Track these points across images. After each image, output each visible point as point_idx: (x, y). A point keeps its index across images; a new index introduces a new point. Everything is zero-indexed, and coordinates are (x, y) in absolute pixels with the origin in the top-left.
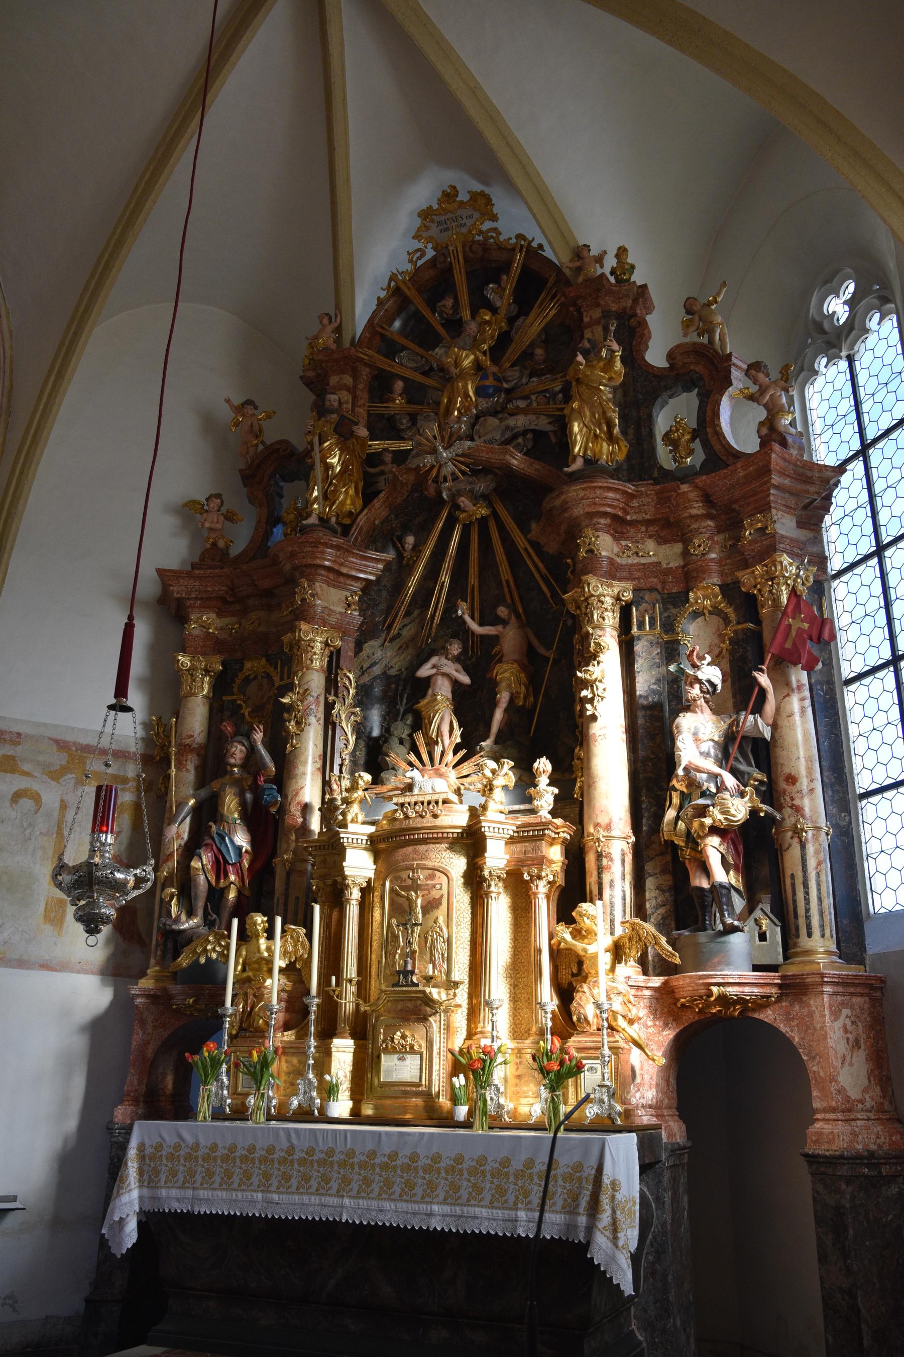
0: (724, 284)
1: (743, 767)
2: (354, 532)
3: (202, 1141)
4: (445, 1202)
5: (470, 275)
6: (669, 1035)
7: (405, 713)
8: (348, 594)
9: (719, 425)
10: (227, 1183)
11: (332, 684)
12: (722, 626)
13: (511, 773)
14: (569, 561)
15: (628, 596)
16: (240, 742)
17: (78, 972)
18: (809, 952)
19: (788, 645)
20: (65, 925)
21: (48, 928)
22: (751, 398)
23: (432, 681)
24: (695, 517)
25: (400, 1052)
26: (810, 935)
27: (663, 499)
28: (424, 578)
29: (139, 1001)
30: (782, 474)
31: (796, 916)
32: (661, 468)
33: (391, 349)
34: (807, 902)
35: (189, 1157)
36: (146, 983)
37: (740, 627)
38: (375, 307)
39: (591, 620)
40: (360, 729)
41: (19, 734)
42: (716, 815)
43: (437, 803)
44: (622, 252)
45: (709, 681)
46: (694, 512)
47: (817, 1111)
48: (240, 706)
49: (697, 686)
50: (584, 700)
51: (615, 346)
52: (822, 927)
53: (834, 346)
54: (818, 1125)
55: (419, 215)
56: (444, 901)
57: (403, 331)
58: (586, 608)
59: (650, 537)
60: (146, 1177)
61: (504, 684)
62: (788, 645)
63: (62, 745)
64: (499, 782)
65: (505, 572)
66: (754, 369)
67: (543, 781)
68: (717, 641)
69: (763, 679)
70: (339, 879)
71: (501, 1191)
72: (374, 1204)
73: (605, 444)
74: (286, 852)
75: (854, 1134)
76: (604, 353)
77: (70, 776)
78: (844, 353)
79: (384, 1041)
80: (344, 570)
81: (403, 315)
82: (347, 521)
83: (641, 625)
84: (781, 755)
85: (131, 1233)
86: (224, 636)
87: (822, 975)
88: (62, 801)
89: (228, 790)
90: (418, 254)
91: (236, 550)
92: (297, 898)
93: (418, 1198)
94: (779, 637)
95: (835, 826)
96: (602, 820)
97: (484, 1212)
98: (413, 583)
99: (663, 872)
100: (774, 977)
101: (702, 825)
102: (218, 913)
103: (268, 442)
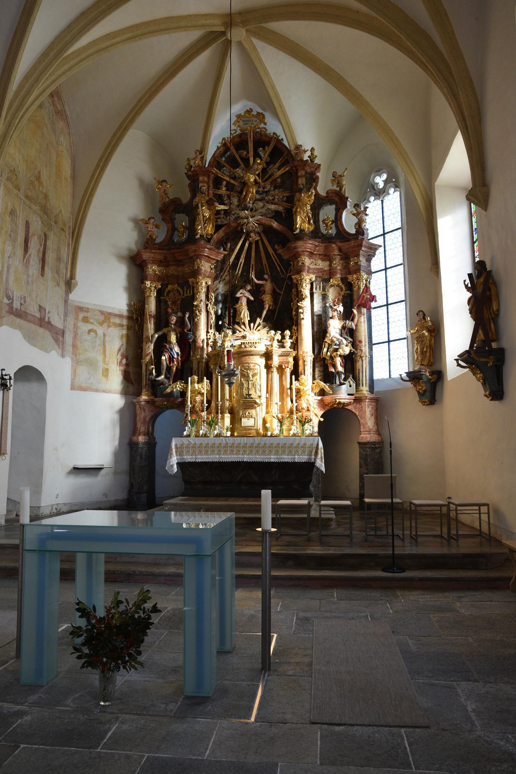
0: (346, 169)
1: (346, 337)
2: (212, 241)
3: (197, 442)
4: (275, 455)
6: (322, 412)
8: (211, 265)
9: (342, 221)
10: (206, 453)
11: (207, 298)
12: (340, 291)
13: (280, 335)
14: (292, 263)
16: (174, 316)
17: (114, 393)
18: (362, 391)
19: (363, 302)
20: (109, 377)
21: (104, 379)
22: (354, 214)
23: (241, 298)
25: (248, 418)
26: (363, 386)
27: (326, 248)
28: (235, 259)
29: (143, 403)
30: (365, 247)
31: (359, 381)
32: (322, 233)
34: (363, 377)
35: (193, 447)
36: (144, 397)
37: (346, 292)
38: (216, 150)
39: (302, 287)
40: (216, 313)
41: (88, 308)
42: (341, 352)
43: (256, 343)
44: (312, 150)
45: (340, 311)
46: (335, 253)
47: (362, 432)
48: (167, 301)
49: (336, 312)
50: (301, 313)
52: (366, 384)
53: (377, 195)
54: (362, 435)
55: (236, 116)
56: (259, 373)
58: (301, 282)
59: (320, 259)
60: (178, 453)
62: (363, 302)
63: (102, 313)
65: (264, 261)
67: (287, 337)
68: (338, 295)
69: (355, 311)
71: (291, 451)
72: (254, 456)
73: (307, 225)
74: (197, 355)
75: (371, 437)
77: (105, 324)
78: (381, 199)
79: (242, 415)
80: (212, 257)
82: (209, 237)
83: (316, 288)
84: (358, 334)
85: (175, 469)
87: (367, 397)
88: (104, 333)
90: (234, 131)
91: (158, 241)
92: (202, 370)
93: (267, 454)
94: (361, 299)
97: (286, 457)
98: (232, 260)
99: (321, 366)
101: (337, 354)
103: (171, 198)
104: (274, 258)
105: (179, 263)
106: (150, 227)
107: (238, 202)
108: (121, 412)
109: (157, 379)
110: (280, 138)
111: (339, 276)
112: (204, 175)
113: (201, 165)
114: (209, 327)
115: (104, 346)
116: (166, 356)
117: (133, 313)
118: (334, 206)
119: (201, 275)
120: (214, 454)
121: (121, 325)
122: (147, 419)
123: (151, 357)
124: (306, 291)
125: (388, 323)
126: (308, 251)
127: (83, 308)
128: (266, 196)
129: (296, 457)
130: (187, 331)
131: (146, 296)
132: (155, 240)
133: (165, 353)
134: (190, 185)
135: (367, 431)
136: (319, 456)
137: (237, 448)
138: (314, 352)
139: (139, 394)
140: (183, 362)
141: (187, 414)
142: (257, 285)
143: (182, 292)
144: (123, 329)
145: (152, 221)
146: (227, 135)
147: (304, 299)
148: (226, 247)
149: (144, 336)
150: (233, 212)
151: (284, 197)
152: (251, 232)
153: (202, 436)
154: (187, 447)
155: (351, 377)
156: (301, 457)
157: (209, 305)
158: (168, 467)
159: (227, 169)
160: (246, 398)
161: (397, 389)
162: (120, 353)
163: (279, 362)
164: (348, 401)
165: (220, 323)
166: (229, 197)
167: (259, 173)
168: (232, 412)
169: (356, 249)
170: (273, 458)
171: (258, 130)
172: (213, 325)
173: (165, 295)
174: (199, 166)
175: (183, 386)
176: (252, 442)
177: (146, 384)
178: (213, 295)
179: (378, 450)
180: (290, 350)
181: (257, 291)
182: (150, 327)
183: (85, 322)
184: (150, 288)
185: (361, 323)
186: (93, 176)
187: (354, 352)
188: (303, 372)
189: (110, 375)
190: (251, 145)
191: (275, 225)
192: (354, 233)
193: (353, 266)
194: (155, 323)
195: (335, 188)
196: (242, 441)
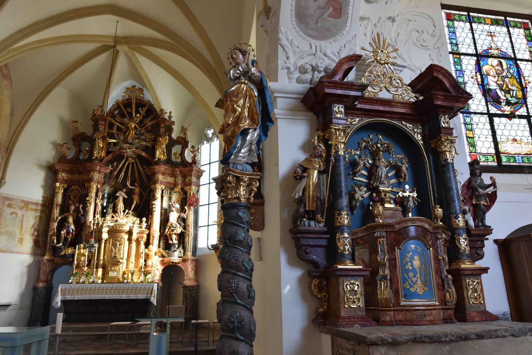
0: (190, 125)
1: (180, 222)
2: (104, 161)
3: (76, 287)
5: (136, 104)
6: (162, 268)
7: (111, 202)
10: (82, 293)
11: (97, 196)
15: (164, 188)
18: (187, 255)
19: (191, 203)
21: (19, 244)
22: (191, 152)
24: (178, 174)
27: (172, 170)
29: (45, 261)
30: (195, 171)
33: (114, 116)
34: (188, 246)
35: (73, 290)
36: (46, 257)
38: (111, 106)
39: (156, 192)
40: (102, 205)
41: (12, 198)
42: (175, 232)
44: (170, 112)
48: (70, 196)
51: (168, 137)
55: (126, 88)
56: (123, 244)
57: (117, 113)
60: (62, 294)
61: (135, 200)
62: (191, 203)
63: (23, 201)
64: (136, 223)
65: (137, 175)
66: (193, 147)
67: (144, 222)
68: (178, 198)
69: (186, 208)
70: (100, 238)
71: (136, 292)
72: (112, 296)
75: (190, 283)
76: (165, 138)
78: (209, 143)
81: (119, 110)
82: (102, 158)
83: (165, 193)
85: (59, 304)
86: (67, 179)
89: (70, 216)
90: (124, 97)
91: (69, 158)
94: (190, 201)
95: (194, 233)
96: (154, 230)
97: (132, 296)
98: (115, 173)
99: (164, 240)
100: (181, 259)
101: (173, 233)
102: (66, 243)
104: (143, 174)
105: (80, 173)
106: (64, 149)
107: (123, 138)
108: (30, 267)
109: (56, 246)
110: (152, 104)
111: (180, 186)
112: (102, 121)
113: (101, 114)
114: (96, 213)
115: (22, 223)
116: (65, 231)
117: (46, 202)
118: (181, 145)
119: (93, 182)
120: (82, 295)
121: (36, 210)
122: (47, 272)
123: (55, 231)
124: (158, 195)
125: (209, 214)
126: (161, 172)
127: (9, 198)
128: (141, 136)
129: (139, 296)
130: (81, 216)
131: (56, 192)
132: (66, 157)
133: (64, 229)
134: (93, 126)
135: (188, 279)
136: (153, 295)
137: (107, 290)
138: (160, 231)
139: (44, 255)
140: (76, 235)
141: (73, 269)
142: (130, 189)
143: (81, 191)
144: (37, 212)
145: (65, 145)
146: (120, 99)
147: (156, 199)
148: (113, 164)
149: (52, 218)
150: (119, 145)
151: (152, 138)
152: (129, 157)
153: (81, 283)
154: (69, 290)
155: (181, 247)
156: (142, 295)
157: (97, 200)
158: (54, 304)
159: (119, 118)
160: (113, 259)
161: (208, 254)
162: (33, 228)
163: (137, 237)
164: (178, 261)
165: (105, 211)
166: (118, 134)
167: (138, 123)
168: (104, 267)
169: (190, 172)
170: (124, 297)
171: (139, 98)
172: (99, 212)
173: (69, 192)
174: (99, 115)
175: (73, 251)
176: (112, 286)
177: (49, 249)
178: (101, 193)
179: (195, 291)
180: (145, 230)
181: (130, 193)
182: (56, 212)
183: (9, 207)
184: (59, 187)
185: (190, 215)
186: (25, 115)
187: (184, 232)
188: (152, 243)
189: (24, 242)
190: (134, 106)
191: (144, 154)
192: (191, 162)
193: (188, 182)
194: (60, 210)
195: (182, 135)
196: (106, 286)
